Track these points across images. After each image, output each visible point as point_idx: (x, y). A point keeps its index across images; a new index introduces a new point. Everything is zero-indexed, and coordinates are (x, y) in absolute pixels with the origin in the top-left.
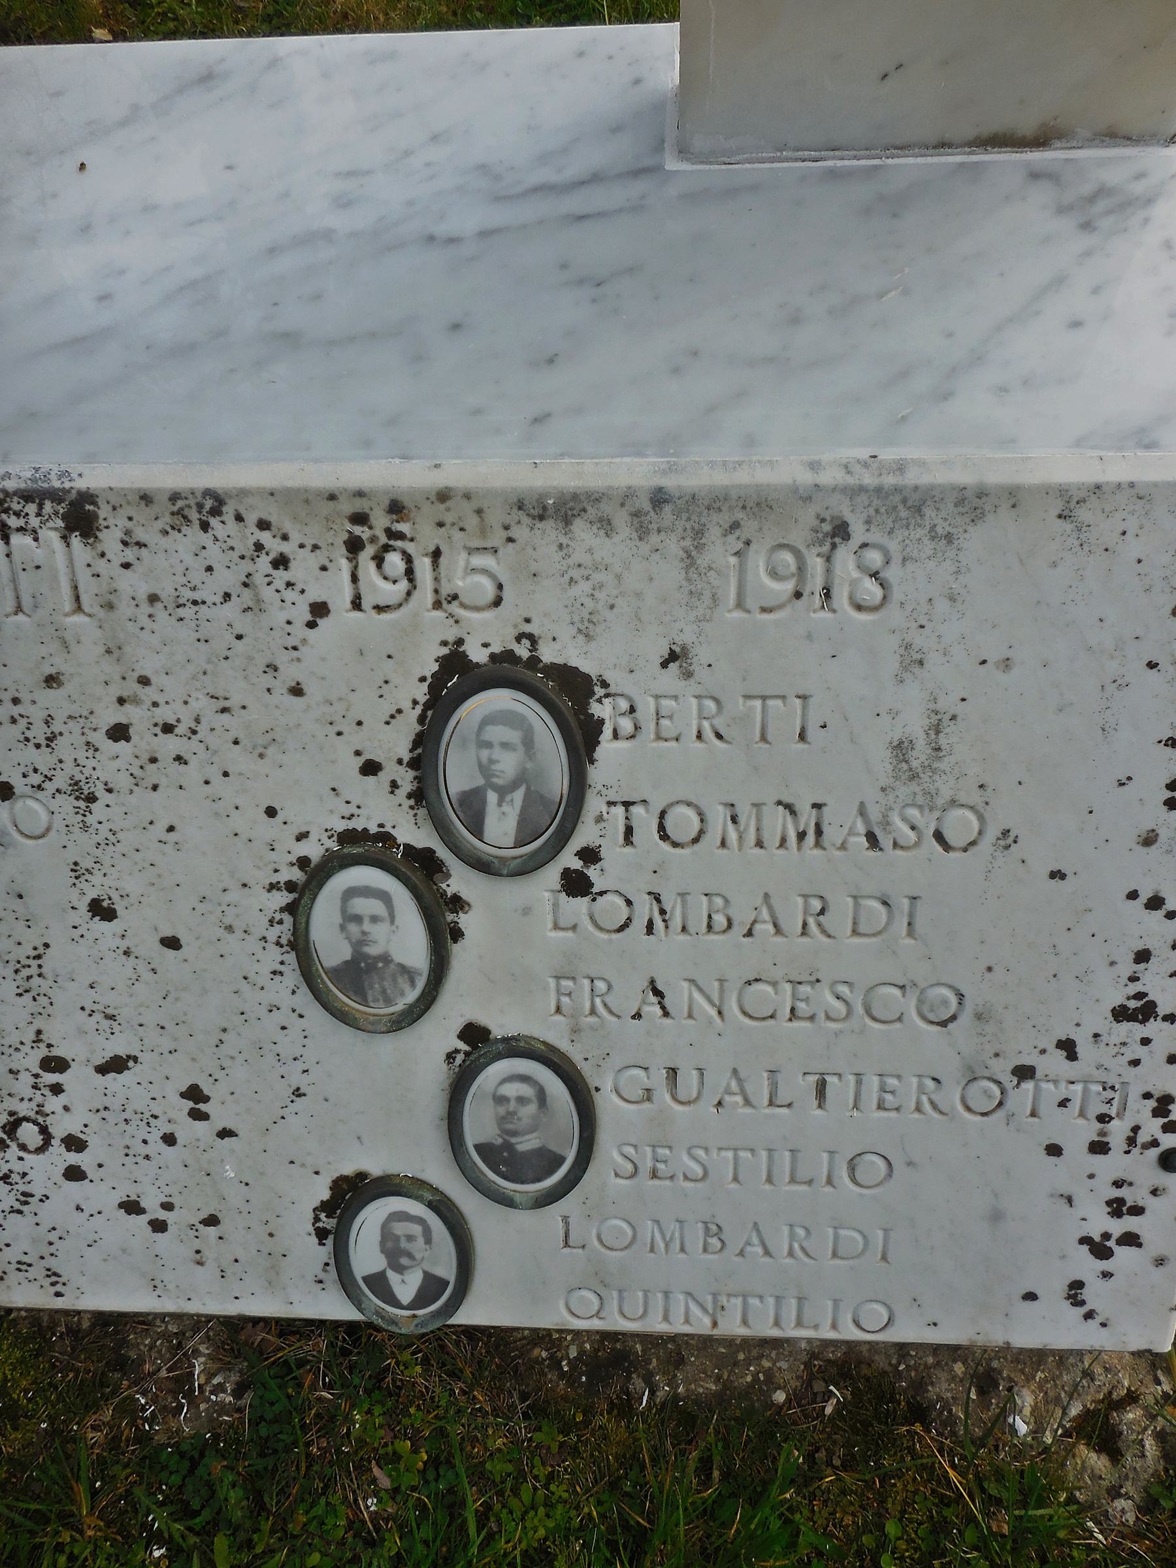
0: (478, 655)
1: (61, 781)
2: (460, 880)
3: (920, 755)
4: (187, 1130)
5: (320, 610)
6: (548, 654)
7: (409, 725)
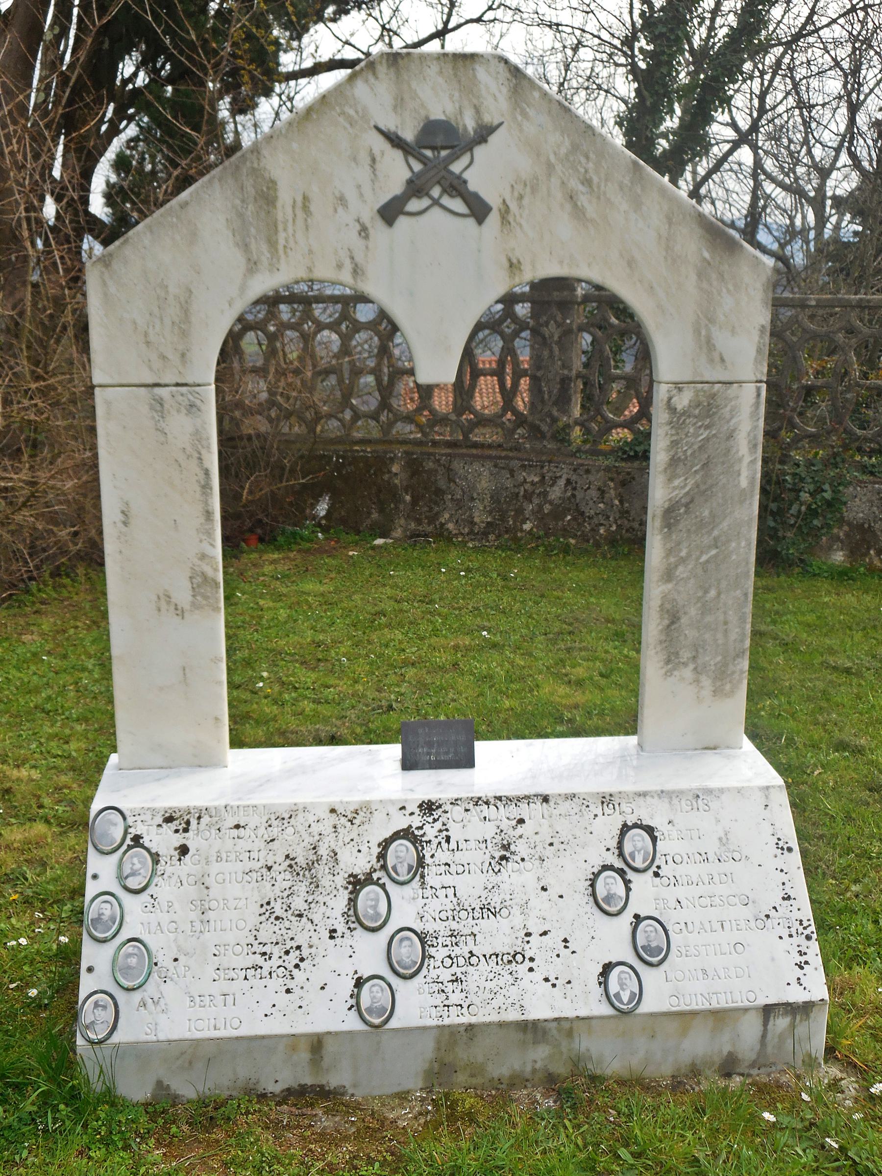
0: (630, 824)
1: (537, 857)
2: (631, 875)
3: (724, 840)
4: (564, 953)
5: (596, 816)
6: (644, 823)
7: (616, 840)
